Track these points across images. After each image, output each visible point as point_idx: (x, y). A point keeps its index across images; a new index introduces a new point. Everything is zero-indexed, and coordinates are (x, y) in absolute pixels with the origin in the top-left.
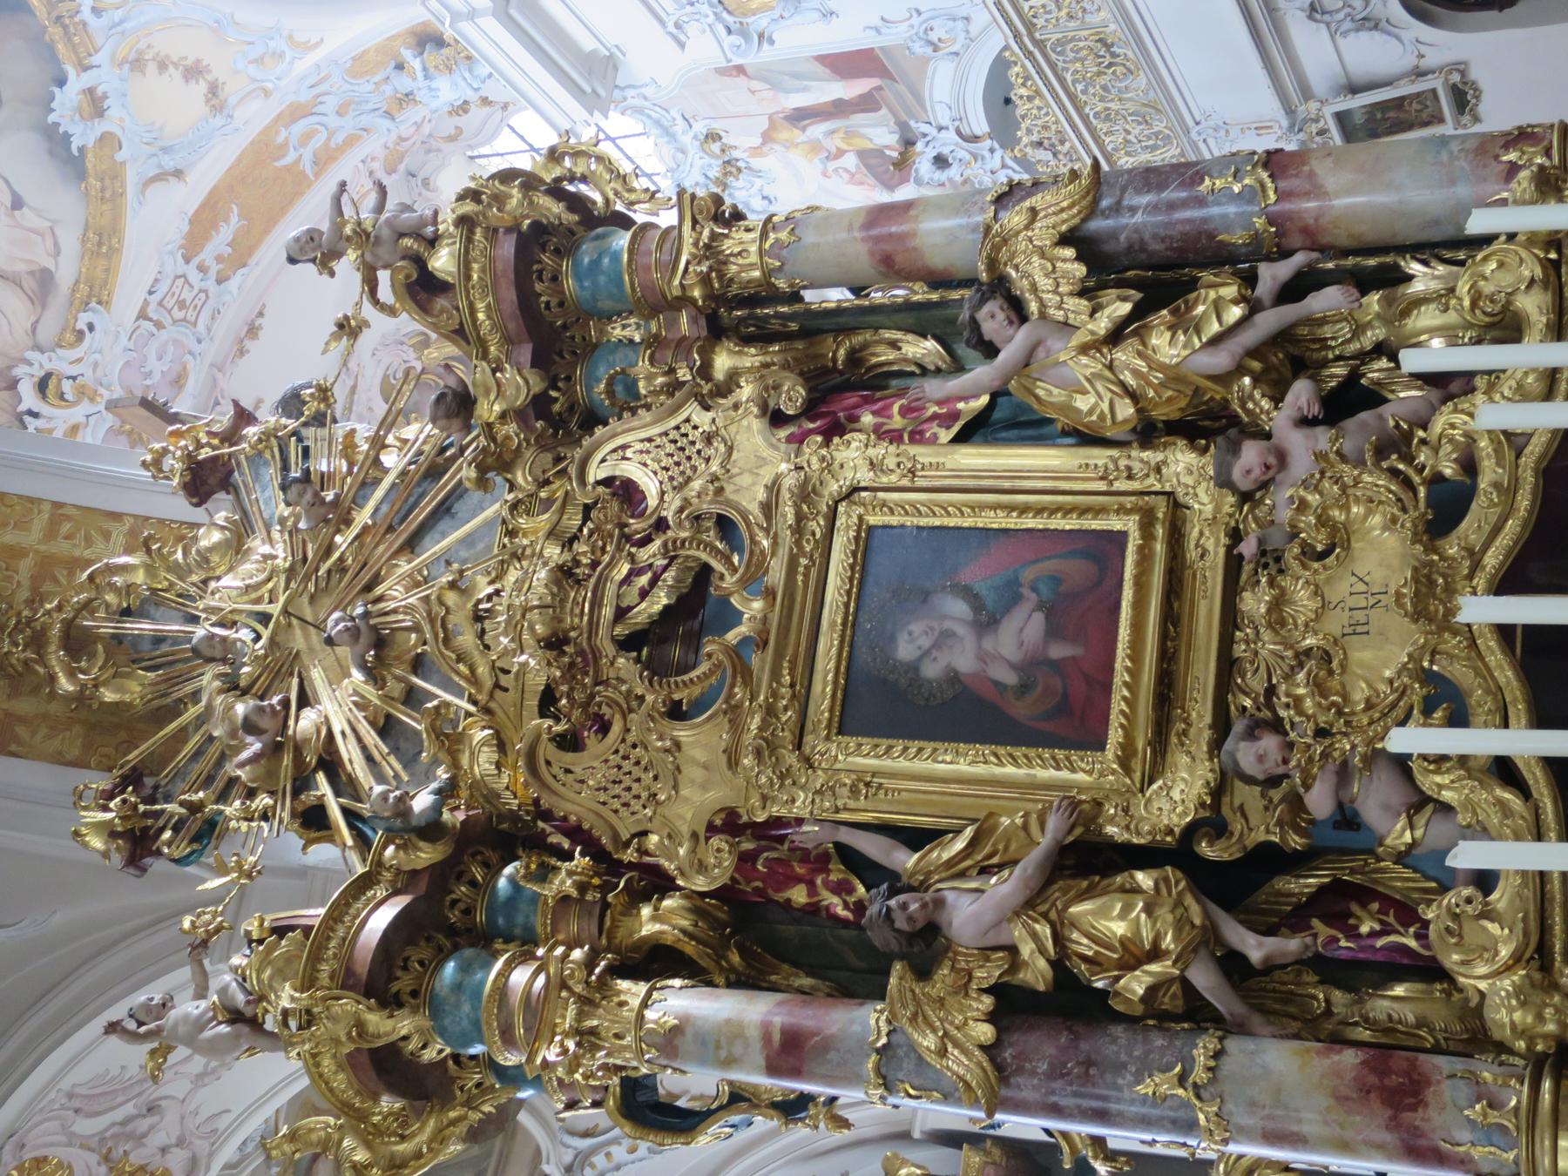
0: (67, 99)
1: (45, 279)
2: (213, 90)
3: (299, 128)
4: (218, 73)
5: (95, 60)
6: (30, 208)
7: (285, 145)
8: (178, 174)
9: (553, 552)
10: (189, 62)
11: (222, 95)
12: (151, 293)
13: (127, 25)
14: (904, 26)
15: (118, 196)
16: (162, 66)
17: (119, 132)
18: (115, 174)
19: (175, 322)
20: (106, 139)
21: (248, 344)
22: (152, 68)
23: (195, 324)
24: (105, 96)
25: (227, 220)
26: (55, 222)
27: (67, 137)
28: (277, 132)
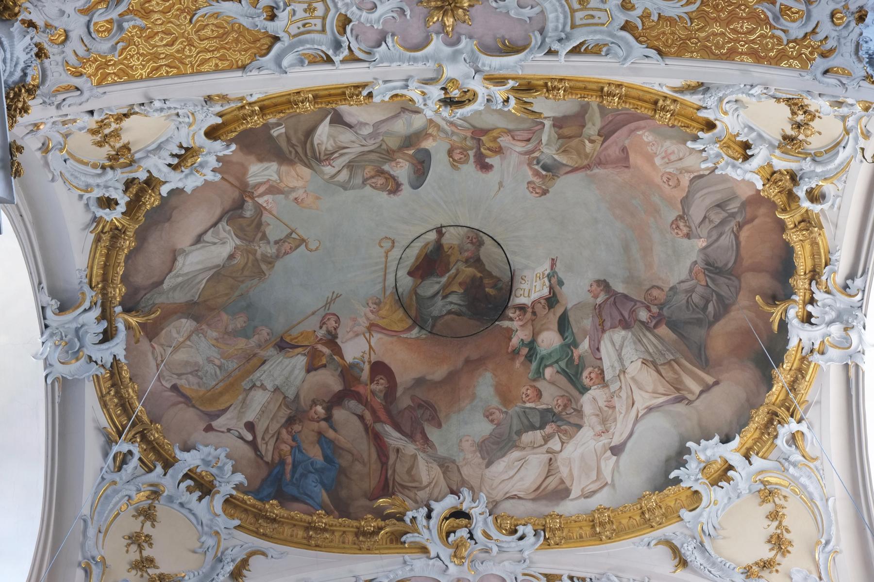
1: (562, 493)
4: (786, 562)
5: (755, 459)
6: (617, 462)
8: (683, 563)
10: (787, 536)
11: (765, 573)
13: (792, 470)
15: (647, 524)
16: (774, 516)
17: (704, 502)
18: (671, 515)
22: (769, 507)
24: (729, 480)
26: (613, 485)
27: (683, 464)
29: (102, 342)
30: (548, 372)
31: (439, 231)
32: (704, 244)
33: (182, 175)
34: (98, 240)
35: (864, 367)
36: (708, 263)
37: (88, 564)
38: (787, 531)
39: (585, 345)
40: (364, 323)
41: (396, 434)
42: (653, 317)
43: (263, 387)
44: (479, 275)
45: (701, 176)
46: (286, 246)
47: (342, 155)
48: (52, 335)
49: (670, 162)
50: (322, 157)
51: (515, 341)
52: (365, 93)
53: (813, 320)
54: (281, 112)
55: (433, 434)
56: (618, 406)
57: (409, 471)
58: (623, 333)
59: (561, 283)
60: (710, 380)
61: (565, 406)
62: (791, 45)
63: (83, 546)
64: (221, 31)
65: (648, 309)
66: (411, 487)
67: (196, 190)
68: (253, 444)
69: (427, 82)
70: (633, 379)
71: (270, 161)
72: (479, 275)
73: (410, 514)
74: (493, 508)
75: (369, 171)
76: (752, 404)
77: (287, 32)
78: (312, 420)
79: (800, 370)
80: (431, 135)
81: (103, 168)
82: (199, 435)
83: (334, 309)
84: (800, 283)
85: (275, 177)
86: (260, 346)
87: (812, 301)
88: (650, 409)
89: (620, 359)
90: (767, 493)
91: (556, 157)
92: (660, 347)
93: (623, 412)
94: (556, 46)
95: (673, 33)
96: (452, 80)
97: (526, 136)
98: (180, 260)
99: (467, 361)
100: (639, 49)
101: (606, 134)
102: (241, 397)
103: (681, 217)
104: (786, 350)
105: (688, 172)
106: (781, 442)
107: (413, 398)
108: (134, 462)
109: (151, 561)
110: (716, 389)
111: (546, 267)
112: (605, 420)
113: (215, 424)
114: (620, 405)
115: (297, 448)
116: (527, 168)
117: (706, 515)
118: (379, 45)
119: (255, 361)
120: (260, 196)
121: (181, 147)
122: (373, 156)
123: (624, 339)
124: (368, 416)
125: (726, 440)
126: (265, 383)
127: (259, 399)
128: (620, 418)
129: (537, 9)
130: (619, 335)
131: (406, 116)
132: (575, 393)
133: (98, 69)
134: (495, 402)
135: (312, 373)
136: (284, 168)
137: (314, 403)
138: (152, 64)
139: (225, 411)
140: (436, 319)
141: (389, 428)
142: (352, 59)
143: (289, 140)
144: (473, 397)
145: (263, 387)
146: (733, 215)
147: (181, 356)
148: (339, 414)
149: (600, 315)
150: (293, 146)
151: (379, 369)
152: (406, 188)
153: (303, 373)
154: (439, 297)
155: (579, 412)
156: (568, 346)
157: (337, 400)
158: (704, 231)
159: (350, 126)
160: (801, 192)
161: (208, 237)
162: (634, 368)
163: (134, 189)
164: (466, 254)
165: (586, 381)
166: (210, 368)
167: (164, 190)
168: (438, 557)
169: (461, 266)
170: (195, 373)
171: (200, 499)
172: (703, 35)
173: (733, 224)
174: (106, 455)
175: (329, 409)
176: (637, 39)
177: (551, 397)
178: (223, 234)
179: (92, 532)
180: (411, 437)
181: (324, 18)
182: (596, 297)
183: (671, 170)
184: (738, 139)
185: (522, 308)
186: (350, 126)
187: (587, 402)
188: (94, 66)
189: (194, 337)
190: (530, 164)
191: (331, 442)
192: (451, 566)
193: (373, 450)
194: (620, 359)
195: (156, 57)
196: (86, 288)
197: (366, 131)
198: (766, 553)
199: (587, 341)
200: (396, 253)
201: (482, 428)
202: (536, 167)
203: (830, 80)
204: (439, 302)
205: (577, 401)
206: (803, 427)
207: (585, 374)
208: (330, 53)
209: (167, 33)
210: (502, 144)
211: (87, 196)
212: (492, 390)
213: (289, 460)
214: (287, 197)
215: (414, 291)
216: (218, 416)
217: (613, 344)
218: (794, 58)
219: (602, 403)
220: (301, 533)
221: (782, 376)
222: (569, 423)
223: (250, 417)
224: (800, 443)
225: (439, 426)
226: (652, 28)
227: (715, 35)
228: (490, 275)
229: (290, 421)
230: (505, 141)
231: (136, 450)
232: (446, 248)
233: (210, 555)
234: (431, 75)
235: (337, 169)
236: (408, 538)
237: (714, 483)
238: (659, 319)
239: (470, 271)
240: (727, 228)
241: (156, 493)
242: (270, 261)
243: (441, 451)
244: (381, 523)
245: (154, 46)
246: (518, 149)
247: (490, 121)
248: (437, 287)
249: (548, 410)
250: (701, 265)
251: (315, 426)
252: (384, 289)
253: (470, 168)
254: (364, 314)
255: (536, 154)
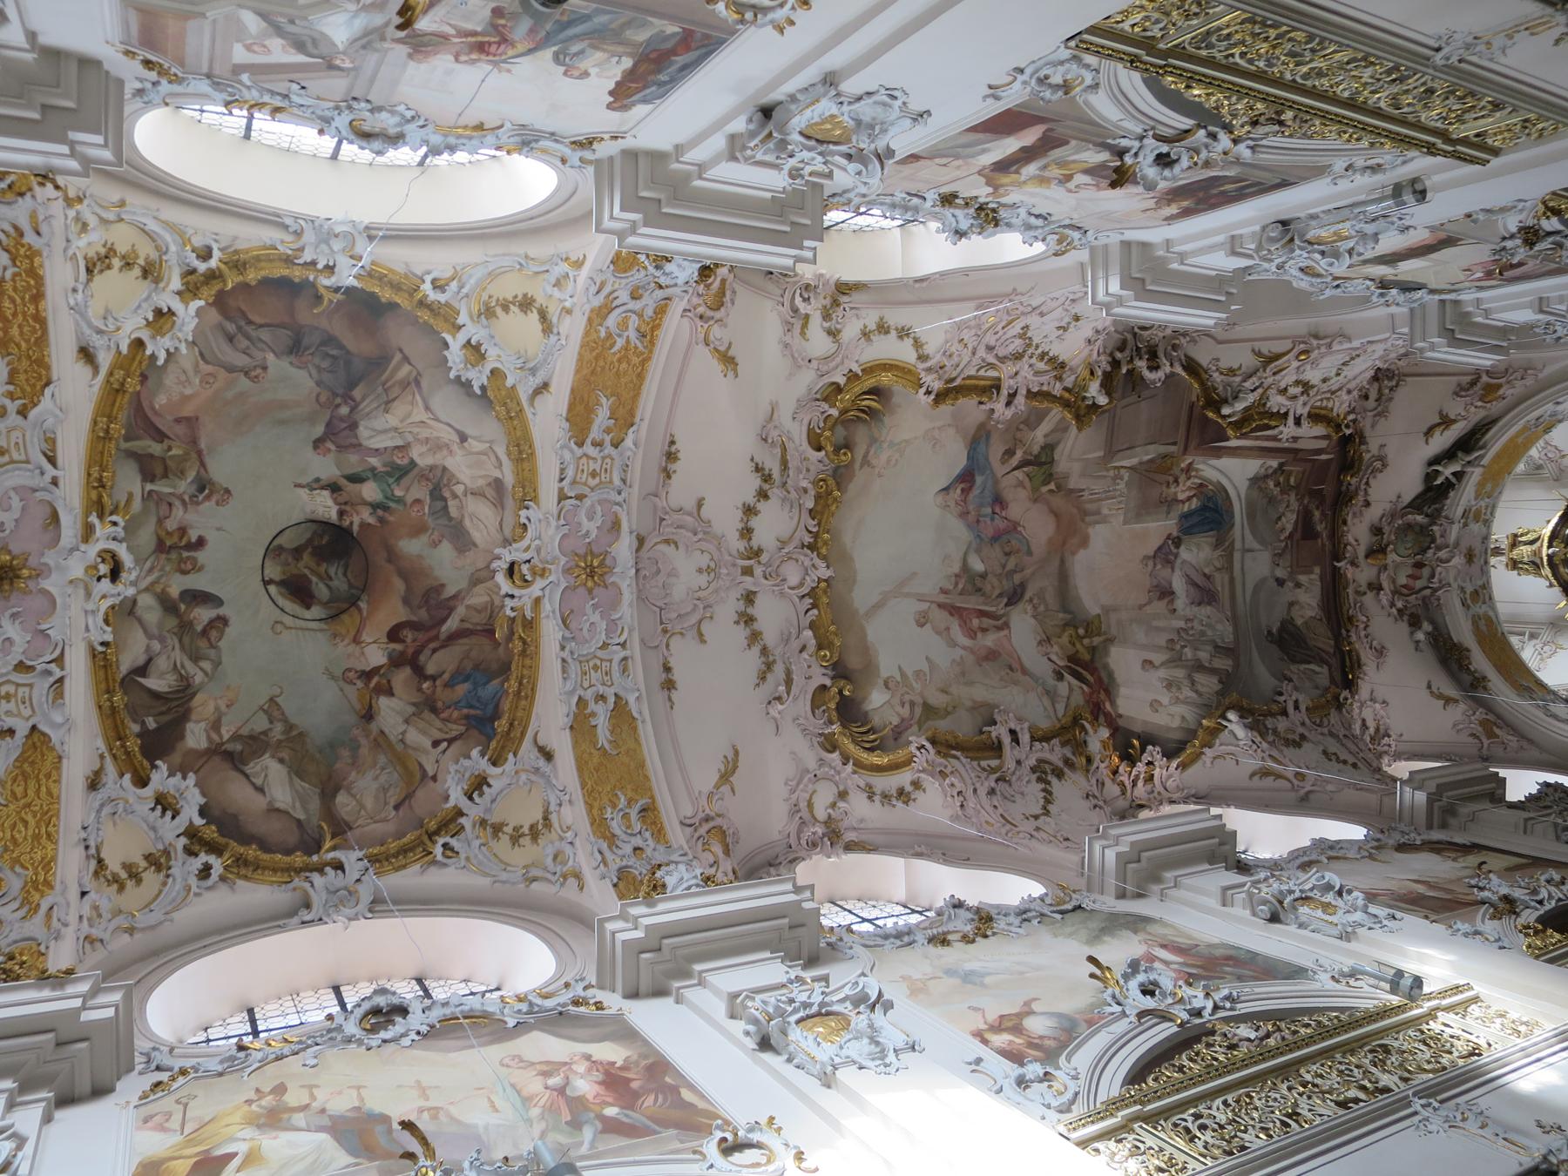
0: (455, 354)
1: (498, 484)
2: (543, 315)
3: (612, 321)
4: (540, 300)
5: (460, 321)
6: (472, 438)
7: (609, 335)
8: (545, 386)
9: (1226, 102)
12: (562, 480)
14: (1017, 85)
19: (592, 489)
20: (495, 373)
21: (672, 467)
22: (499, 310)
23: (611, 482)
24: (479, 345)
25: (599, 403)
26: (491, 442)
28: (597, 332)
29: (344, 871)
30: (398, 493)
31: (266, 583)
32: (272, 355)
33: (186, 806)
34: (246, 878)
35: (366, 222)
36: (291, 352)
37: (526, 880)
38: (516, 297)
39: (374, 461)
40: (352, 648)
41: (449, 622)
42: (346, 403)
43: (403, 733)
44: (310, 550)
45: (201, 354)
46: (276, 713)
47: (183, 666)
48: (329, 915)
49: (188, 380)
50: (185, 683)
51: (371, 520)
52: (101, 649)
53: (331, 264)
54: (123, 722)
55: (450, 591)
56: (425, 435)
57: (479, 612)
58: (361, 428)
59: (317, 480)
60: (398, 356)
61: (428, 479)
62: (18, 263)
63: (514, 884)
64: (20, 778)
65: (338, 406)
66: (492, 611)
67: (204, 794)
68: (450, 741)
69: (88, 594)
70: (402, 421)
71: (184, 729)
72: (310, 550)
73: (509, 612)
74: (507, 542)
75: (203, 644)
76: (415, 321)
77: (28, 719)
78: (434, 692)
79: (380, 279)
80: (163, 590)
81: (168, 876)
82: (438, 787)
83: (338, 672)
84: (297, 274)
85: (203, 725)
86: (367, 736)
87: (314, 263)
88: (427, 408)
89: (385, 431)
90: (488, 312)
91: (189, 480)
92: (372, 397)
93: (430, 431)
94: (48, 478)
95: (26, 371)
96: (88, 569)
97: (164, 507)
98: (278, 805)
99: (389, 561)
100: (46, 402)
101: (160, 436)
102: (410, 752)
103: (246, 374)
104: (362, 290)
105: (197, 365)
106: (442, 298)
107: (420, 607)
108: (453, 842)
109: (532, 827)
110: (406, 351)
111: (303, 493)
112: (438, 446)
113: (431, 773)
114: (424, 433)
115: (456, 705)
116: (201, 507)
117: (509, 367)
118: (48, 636)
119: (380, 740)
120: (221, 737)
121: (153, 809)
122: (186, 639)
123: (366, 428)
124: (433, 645)
125: (446, 346)
126: (401, 730)
127: (414, 736)
128: (435, 434)
129: (12, 494)
130: (363, 432)
131: (139, 611)
132: (415, 471)
133: (37, 889)
134: (424, 538)
135: (395, 691)
136: (194, 716)
137: (420, 690)
138: (44, 840)
139: (421, 766)
140: (351, 586)
141: (444, 628)
142: (59, 660)
143: (162, 713)
144: (420, 557)
145: (403, 733)
146: (240, 328)
147: (369, 803)
148: (431, 669)
149: (346, 447)
150: (170, 710)
151: (394, 635)
152: (221, 611)
153: (393, 699)
154: (330, 583)
155: (432, 468)
156: (375, 475)
157: (419, 671)
158: (258, 355)
159: (149, 661)
160: (202, 267)
161: (258, 782)
162: (392, 420)
163: (196, 848)
164: (290, 560)
165: (406, 461)
166: (383, 779)
167: (199, 821)
168: (543, 589)
169: (301, 564)
170: (385, 790)
171: (489, 786)
172: (23, 345)
173: (249, 329)
174: (445, 865)
175: (426, 678)
176: (35, 405)
177: (420, 492)
178: (258, 768)
179: (504, 876)
180: (451, 610)
181: (18, 685)
182: (329, 450)
183: (197, 381)
184: (151, 319)
185: (341, 513)
186: (149, 661)
187: (423, 462)
188: (33, 892)
189: (353, 791)
190: (198, 504)
191: (452, 677)
192: (551, 579)
193: (461, 641)
194: (385, 431)
195: (37, 837)
196: (291, 886)
197: (156, 646)
198: (909, 342)
199: (370, 460)
200: (288, 620)
201: (446, 550)
202: (201, 498)
203: (44, 228)
204: (335, 583)
205: (422, 469)
206: (428, 279)
207: (399, 462)
208: (52, 680)
209: (14, 826)
210: (175, 527)
211: (194, 889)
212: (414, 541)
213: (465, 711)
214: (225, 714)
215: (325, 605)
216: (425, 771)
217: (371, 437)
218: (32, 262)
219: (424, 449)
220: (523, 703)
221: (386, 295)
222: (442, 477)
223: (428, 743)
224: (442, 282)
225: (443, 586)
226: (23, 391)
227: (21, 334)
228: (310, 541)
229: (434, 710)
230: (171, 525)
231: (441, 841)
232: (283, 577)
233: (533, 778)
234: (82, 592)
235: (198, 670)
236: (529, 614)
237: (483, 357)
238: (347, 397)
239: (306, 557)
240: (253, 334)
241: (483, 823)
242: (290, 727)
243: (464, 584)
244: (516, 636)
245: (25, 838)
246: (181, 513)
247: (146, 536)
248: (321, 586)
249: (431, 493)
250: (292, 358)
251: (439, 689)
252: (321, 630)
253: (201, 556)
254: (344, 648)
255: (186, 498)
